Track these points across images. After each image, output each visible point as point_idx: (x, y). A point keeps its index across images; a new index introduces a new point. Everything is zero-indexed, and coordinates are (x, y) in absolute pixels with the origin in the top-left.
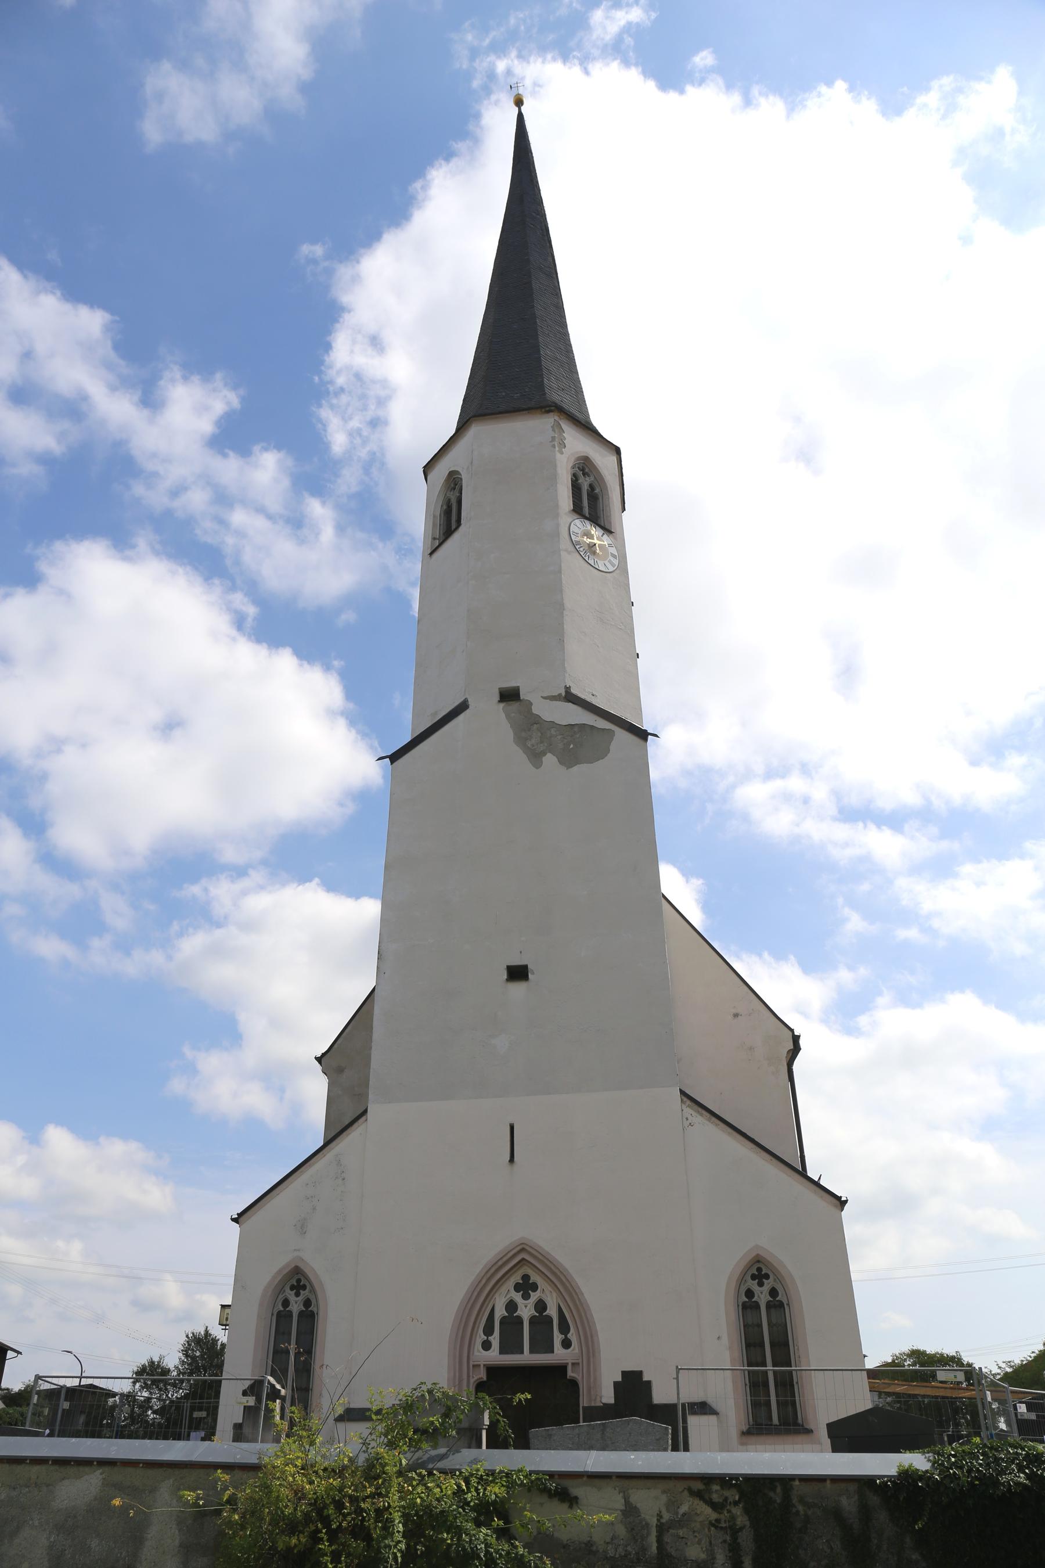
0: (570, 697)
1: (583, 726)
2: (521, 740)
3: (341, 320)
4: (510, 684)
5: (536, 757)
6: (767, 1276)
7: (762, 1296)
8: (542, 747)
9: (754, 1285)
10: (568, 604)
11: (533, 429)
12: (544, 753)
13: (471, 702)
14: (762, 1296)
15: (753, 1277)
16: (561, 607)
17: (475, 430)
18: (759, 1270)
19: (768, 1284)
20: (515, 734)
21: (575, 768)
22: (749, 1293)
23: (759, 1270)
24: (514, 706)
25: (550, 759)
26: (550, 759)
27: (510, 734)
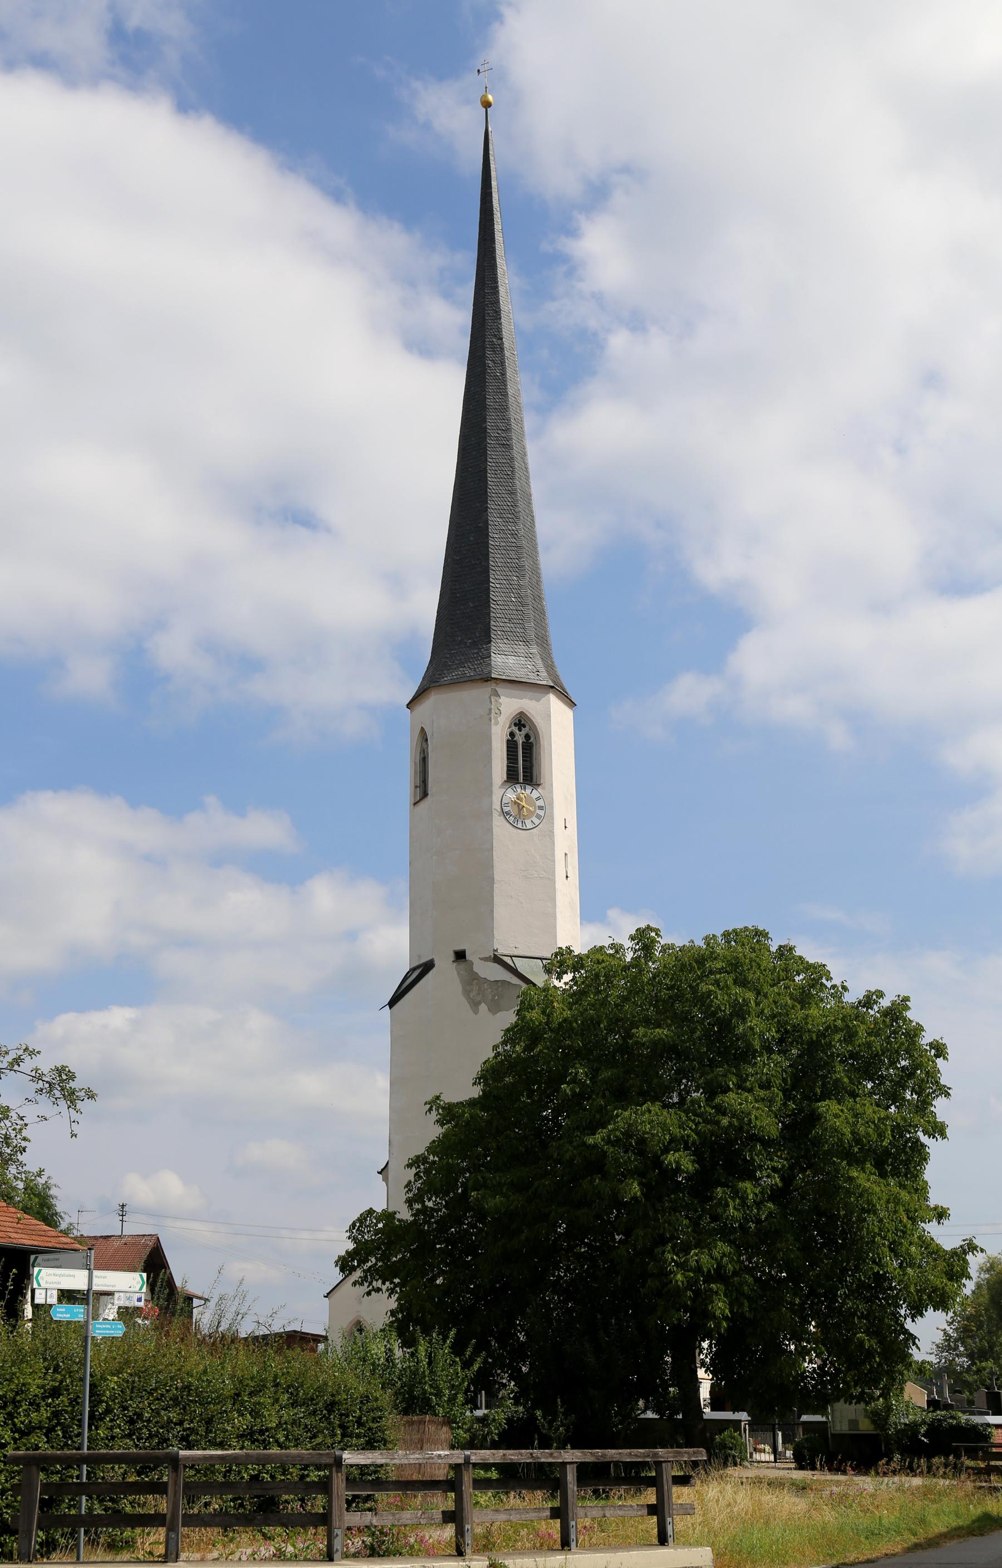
0: (497, 959)
1: (503, 982)
2: (466, 993)
3: (430, 1130)
4: (459, 948)
5: (475, 1005)
6: (524, 726)
7: (520, 739)
8: (479, 998)
9: (516, 730)
10: (497, 877)
11: (471, 696)
12: (479, 1003)
13: (436, 962)
14: (520, 739)
15: (515, 725)
16: (491, 880)
17: (433, 699)
18: (520, 721)
19: (524, 731)
20: (463, 988)
21: (498, 1014)
22: (512, 734)
23: (520, 721)
24: (462, 965)
25: (483, 1007)
26: (483, 1007)
27: (460, 989)
